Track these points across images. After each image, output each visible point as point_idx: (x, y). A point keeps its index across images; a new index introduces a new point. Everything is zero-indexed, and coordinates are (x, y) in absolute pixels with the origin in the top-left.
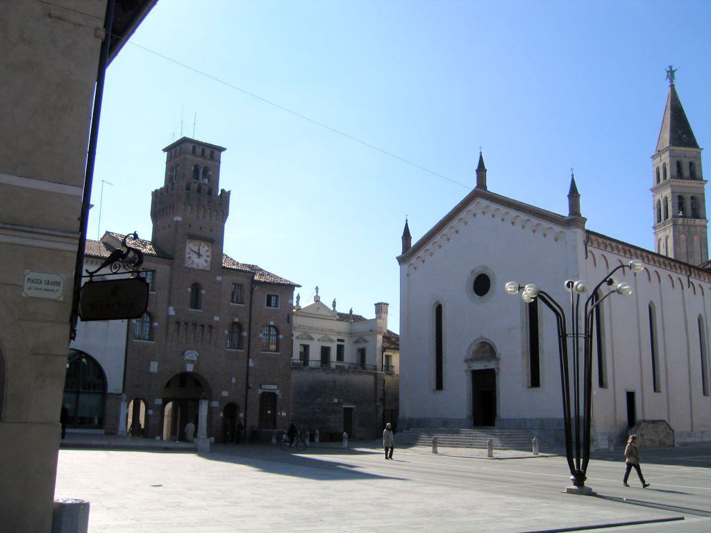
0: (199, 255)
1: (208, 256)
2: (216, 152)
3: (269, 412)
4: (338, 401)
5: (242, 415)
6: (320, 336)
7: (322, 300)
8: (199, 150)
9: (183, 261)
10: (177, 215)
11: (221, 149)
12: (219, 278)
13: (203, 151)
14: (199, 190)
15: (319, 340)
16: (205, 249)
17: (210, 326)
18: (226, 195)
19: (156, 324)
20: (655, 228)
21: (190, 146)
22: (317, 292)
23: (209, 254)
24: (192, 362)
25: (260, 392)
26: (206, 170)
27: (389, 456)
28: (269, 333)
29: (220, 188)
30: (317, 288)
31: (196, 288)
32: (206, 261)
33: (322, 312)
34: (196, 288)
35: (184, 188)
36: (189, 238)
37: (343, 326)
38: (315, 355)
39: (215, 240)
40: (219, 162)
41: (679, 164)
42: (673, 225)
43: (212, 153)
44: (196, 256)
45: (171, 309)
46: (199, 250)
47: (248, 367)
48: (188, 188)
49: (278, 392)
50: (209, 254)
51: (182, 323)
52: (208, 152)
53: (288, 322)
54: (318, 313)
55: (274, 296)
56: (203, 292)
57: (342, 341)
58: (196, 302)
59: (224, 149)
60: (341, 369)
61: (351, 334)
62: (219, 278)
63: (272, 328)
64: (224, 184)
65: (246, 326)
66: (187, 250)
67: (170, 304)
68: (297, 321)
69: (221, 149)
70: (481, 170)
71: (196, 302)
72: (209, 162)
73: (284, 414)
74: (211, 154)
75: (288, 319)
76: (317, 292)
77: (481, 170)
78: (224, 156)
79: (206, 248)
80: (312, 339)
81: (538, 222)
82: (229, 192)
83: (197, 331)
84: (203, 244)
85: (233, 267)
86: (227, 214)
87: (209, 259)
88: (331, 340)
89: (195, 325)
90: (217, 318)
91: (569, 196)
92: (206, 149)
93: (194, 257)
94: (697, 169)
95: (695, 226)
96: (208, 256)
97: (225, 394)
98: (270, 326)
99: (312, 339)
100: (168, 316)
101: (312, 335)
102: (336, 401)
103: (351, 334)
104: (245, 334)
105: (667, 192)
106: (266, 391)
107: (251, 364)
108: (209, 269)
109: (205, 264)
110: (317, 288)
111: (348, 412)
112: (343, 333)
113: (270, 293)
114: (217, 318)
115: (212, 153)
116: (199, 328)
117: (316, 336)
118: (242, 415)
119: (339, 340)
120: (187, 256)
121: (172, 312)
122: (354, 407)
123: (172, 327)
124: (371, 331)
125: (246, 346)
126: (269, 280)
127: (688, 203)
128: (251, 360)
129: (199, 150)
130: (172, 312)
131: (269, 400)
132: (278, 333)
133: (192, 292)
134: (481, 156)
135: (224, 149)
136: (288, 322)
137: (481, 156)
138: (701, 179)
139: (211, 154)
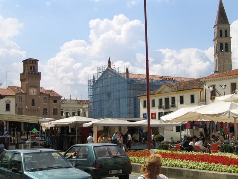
1: (36, 91)
6: (72, 109)
9: (29, 93)
10: (26, 81)
11: (38, 60)
12: (39, 97)
14: (32, 74)
17: (38, 110)
18: (39, 74)
19: (23, 111)
20: (214, 55)
21: (29, 61)
26: (34, 67)
29: (38, 72)
30: (70, 95)
31: (33, 100)
34: (33, 100)
35: (28, 74)
36: (30, 87)
39: (37, 86)
41: (221, 31)
42: (218, 55)
43: (35, 62)
45: (27, 106)
48: (29, 73)
51: (30, 110)
53: (60, 107)
56: (35, 101)
58: (33, 104)
59: (38, 60)
62: (39, 97)
64: (39, 71)
65: (48, 109)
67: (26, 105)
69: (38, 60)
70: (109, 62)
71: (33, 104)
72: (35, 65)
74: (35, 62)
75: (60, 105)
77: (109, 62)
78: (39, 62)
79: (35, 89)
82: (41, 73)
83: (30, 112)
84: (34, 88)
86: (40, 79)
87: (36, 92)
89: (33, 110)
90: (39, 108)
94: (228, 32)
95: (226, 55)
96: (36, 91)
99: (69, 110)
100: (26, 109)
104: (48, 111)
105: (216, 42)
108: (36, 95)
110: (70, 95)
114: (39, 108)
115: (35, 62)
116: (32, 111)
119: (78, 110)
121: (27, 107)
123: (27, 111)
125: (48, 114)
126: (55, 95)
127: (224, 46)
130: (27, 107)
132: (22, 110)
133: (32, 102)
134: (109, 58)
135: (38, 60)
136: (60, 107)
137: (109, 58)
138: (230, 37)
139: (35, 62)
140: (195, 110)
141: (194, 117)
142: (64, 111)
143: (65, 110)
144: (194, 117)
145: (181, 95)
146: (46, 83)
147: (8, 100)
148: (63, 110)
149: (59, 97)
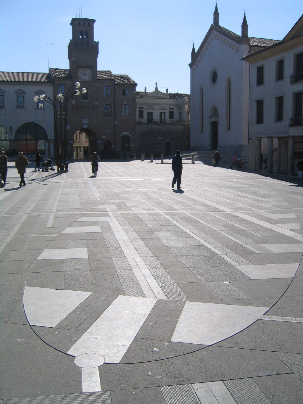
0: (85, 75)
1: (90, 75)
2: (91, 23)
3: (127, 145)
4: (162, 138)
5: (113, 146)
7: (159, 90)
8: (82, 23)
11: (94, 21)
13: (84, 23)
15: (158, 109)
16: (88, 72)
22: (157, 85)
23: (90, 73)
24: (86, 124)
25: (121, 136)
27: (152, 161)
28: (107, 108)
29: (94, 41)
30: (156, 84)
32: (89, 77)
33: (159, 95)
37: (172, 101)
38: (156, 117)
40: (93, 27)
43: (89, 24)
44: (83, 75)
46: (85, 72)
47: (115, 124)
49: (130, 135)
50: (90, 73)
52: (87, 23)
53: (134, 102)
54: (157, 96)
55: (127, 90)
57: (173, 109)
60: (173, 124)
61: (176, 105)
62: (96, 85)
63: (108, 105)
64: (96, 39)
66: (79, 73)
68: (138, 100)
69: (94, 21)
70: (216, 14)
73: (133, 146)
74: (89, 23)
76: (157, 85)
77: (216, 14)
78: (95, 25)
79: (89, 71)
80: (154, 109)
81: (229, 40)
84: (87, 69)
85: (108, 78)
87: (90, 76)
88: (165, 109)
90: (96, 103)
91: (242, 26)
92: (86, 22)
93: (83, 76)
96: (90, 75)
97: (104, 137)
98: (107, 105)
99: (154, 109)
101: (154, 107)
102: (160, 138)
103: (176, 105)
106: (124, 135)
107: (116, 123)
109: (89, 79)
110: (156, 84)
111: (167, 144)
112: (172, 105)
113: (125, 89)
114: (96, 103)
117: (156, 108)
118: (113, 146)
119: (170, 109)
120: (79, 76)
122: (171, 141)
124: (182, 103)
128: (116, 121)
129: (82, 23)
131: (126, 139)
136: (134, 102)
139: (89, 23)
140: (198, 182)
141: (300, 199)
142: (144, 109)
143: (146, 109)
144: (300, 199)
145: (259, 64)
146: (108, 62)
147: (20, 90)
148: (143, 108)
149: (134, 84)
